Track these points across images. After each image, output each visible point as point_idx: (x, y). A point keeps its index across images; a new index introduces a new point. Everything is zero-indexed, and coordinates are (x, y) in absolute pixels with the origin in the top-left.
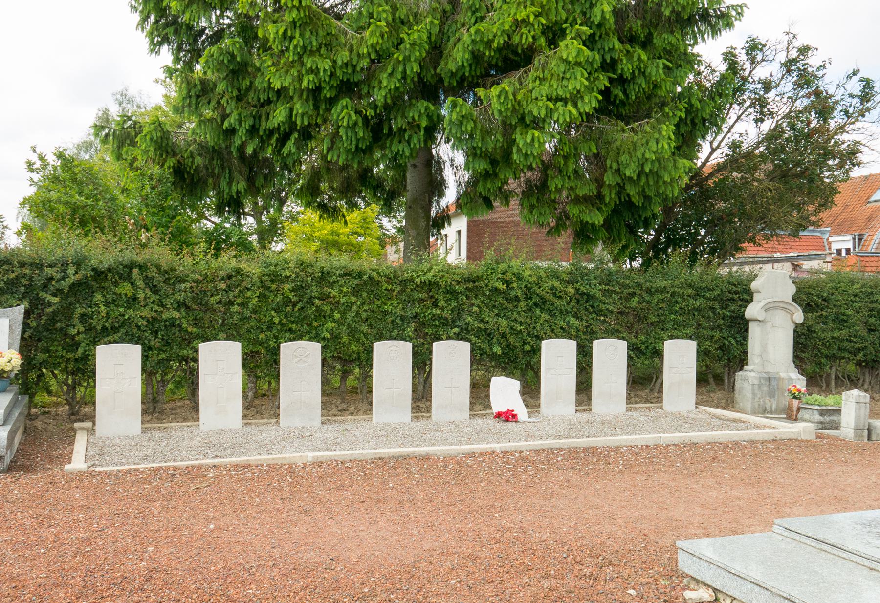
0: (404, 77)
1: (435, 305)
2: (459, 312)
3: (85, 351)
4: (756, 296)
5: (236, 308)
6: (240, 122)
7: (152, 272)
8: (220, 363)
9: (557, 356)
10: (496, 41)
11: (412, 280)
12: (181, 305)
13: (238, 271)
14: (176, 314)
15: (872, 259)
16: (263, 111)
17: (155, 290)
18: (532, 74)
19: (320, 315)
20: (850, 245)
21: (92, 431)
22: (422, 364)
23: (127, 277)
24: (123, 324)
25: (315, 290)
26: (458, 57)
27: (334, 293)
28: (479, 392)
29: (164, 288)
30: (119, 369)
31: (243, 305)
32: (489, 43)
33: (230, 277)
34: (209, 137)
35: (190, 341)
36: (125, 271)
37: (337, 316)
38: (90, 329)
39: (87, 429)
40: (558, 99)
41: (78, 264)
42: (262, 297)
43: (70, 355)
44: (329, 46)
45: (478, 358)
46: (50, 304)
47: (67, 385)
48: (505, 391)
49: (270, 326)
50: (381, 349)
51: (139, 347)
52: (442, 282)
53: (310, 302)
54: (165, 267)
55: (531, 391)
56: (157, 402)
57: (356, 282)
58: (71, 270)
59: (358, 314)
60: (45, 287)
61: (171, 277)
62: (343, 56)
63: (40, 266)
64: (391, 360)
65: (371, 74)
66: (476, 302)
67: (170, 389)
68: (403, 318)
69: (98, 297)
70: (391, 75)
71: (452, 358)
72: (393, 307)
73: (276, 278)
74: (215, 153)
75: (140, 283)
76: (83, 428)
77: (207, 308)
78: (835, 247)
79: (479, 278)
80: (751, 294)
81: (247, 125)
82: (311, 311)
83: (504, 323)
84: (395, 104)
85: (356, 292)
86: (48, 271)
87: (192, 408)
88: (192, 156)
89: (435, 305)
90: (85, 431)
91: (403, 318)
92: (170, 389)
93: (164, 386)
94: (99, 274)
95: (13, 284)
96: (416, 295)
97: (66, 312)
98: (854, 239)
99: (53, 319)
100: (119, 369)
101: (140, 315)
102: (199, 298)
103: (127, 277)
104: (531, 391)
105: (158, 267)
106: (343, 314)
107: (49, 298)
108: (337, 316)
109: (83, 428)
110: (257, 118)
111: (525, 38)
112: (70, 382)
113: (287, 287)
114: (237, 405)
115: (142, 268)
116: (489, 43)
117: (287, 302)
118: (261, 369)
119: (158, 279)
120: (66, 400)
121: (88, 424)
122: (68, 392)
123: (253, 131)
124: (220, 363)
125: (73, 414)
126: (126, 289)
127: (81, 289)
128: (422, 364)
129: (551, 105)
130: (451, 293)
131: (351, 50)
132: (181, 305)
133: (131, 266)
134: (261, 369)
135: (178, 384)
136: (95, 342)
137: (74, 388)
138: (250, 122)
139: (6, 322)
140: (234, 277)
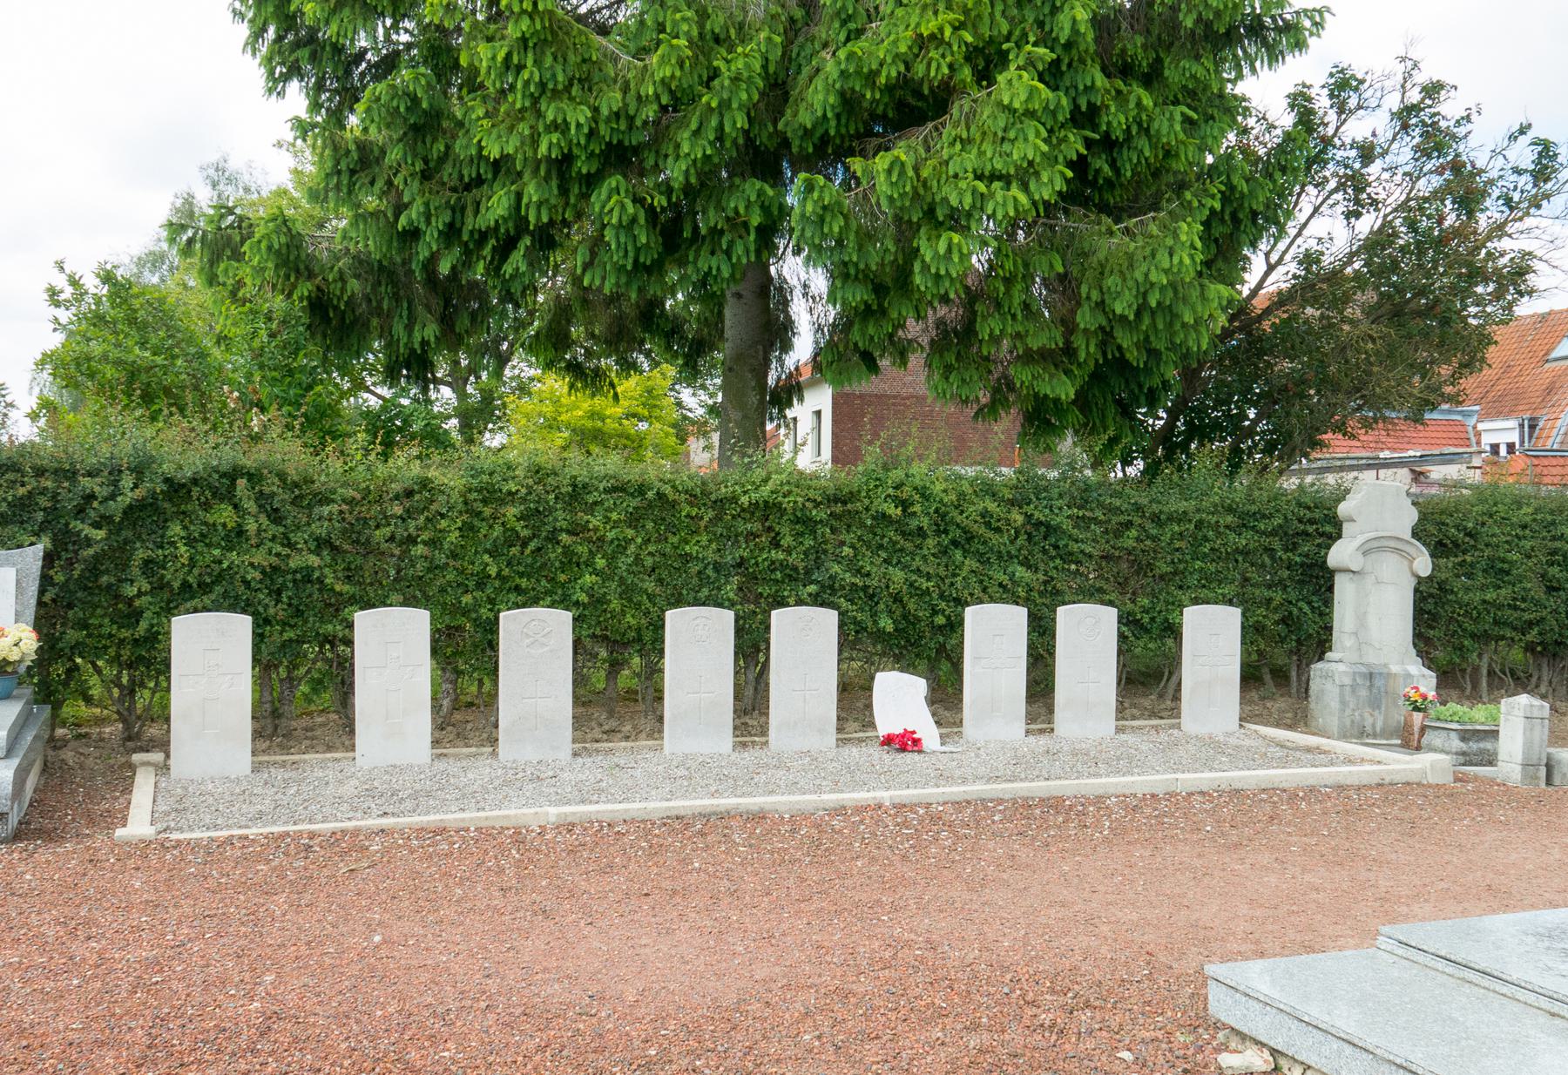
0: (720, 137)
1: (776, 544)
2: (818, 555)
3: (152, 626)
4: (1347, 528)
5: (420, 550)
6: (428, 217)
7: (272, 485)
8: (392, 647)
9: (993, 635)
10: (884, 74)
11: (734, 499)
12: (322, 544)
13: (425, 484)
14: (314, 560)
15: (1554, 462)
16: (469, 198)
17: (276, 516)
18: (948, 132)
19: (571, 561)
20: (1514, 437)
21: (163, 769)
22: (752, 649)
23: (226, 494)
24: (219, 578)
25: (561, 518)
26: (815, 101)
27: (595, 522)
28: (854, 698)
29: (293, 514)
30: (211, 657)
31: (433, 543)
32: (872, 76)
33: (409, 493)
34: (372, 245)
35: (338, 608)
36: (223, 484)
37: (600, 562)
38: (160, 586)
39: (155, 765)
40: (994, 177)
41: (139, 471)
42: (467, 530)
43: (125, 633)
44: (586, 82)
45: (851, 638)
46: (88, 542)
47: (119, 685)
48: (900, 697)
49: (482, 581)
50: (678, 622)
51: (248, 619)
52: (787, 503)
53: (553, 538)
54: (293, 475)
55: (946, 696)
56: (279, 716)
57: (635, 502)
58: (127, 481)
59: (638, 560)
60: (80, 512)
61: (305, 494)
62: (612, 99)
63: (71, 475)
64: (697, 641)
65: (661, 133)
66: (849, 538)
67: (303, 693)
68: (717, 567)
69: (176, 529)
70: (697, 133)
71: (805, 638)
72: (701, 547)
73: (492, 495)
74: (383, 274)
75: (250, 506)
76: (148, 764)
77: (369, 549)
78: (1487, 440)
79: (853, 496)
80: (1338, 525)
81: (440, 222)
82: (555, 554)
83: (898, 575)
84: (703, 186)
85: (634, 520)
86: (86, 483)
87: (342, 727)
88: (342, 278)
89: (776, 544)
90: (151, 769)
91: (717, 567)
92: (303, 693)
93: (292, 688)
94: (176, 489)
95: (23, 506)
96: (743, 527)
97: (118, 555)
98: (1522, 426)
99: (94, 568)
100: (211, 657)
101: (251, 561)
102: (356, 532)
103: (226, 494)
104: (946, 696)
105: (282, 476)
106: (611, 559)
107: (88, 531)
108: (600, 562)
109: (148, 764)
110: (458, 210)
111: (935, 67)
112: (125, 680)
113: (512, 511)
114: (422, 722)
115: (254, 477)
116: (872, 76)
117: (512, 538)
118: (465, 659)
119: (282, 497)
120: (118, 712)
121: (157, 757)
122: (121, 700)
123: (451, 233)
124: (392, 647)
125: (129, 738)
126: (224, 515)
127: (145, 515)
128: (752, 649)
129: (981, 187)
130: (804, 523)
131: (625, 89)
132: (322, 544)
133: (233, 474)
134: (465, 659)
135: (318, 685)
136: (169, 610)
137: (132, 692)
138: (446, 217)
139: (10, 574)
140: (418, 493)
